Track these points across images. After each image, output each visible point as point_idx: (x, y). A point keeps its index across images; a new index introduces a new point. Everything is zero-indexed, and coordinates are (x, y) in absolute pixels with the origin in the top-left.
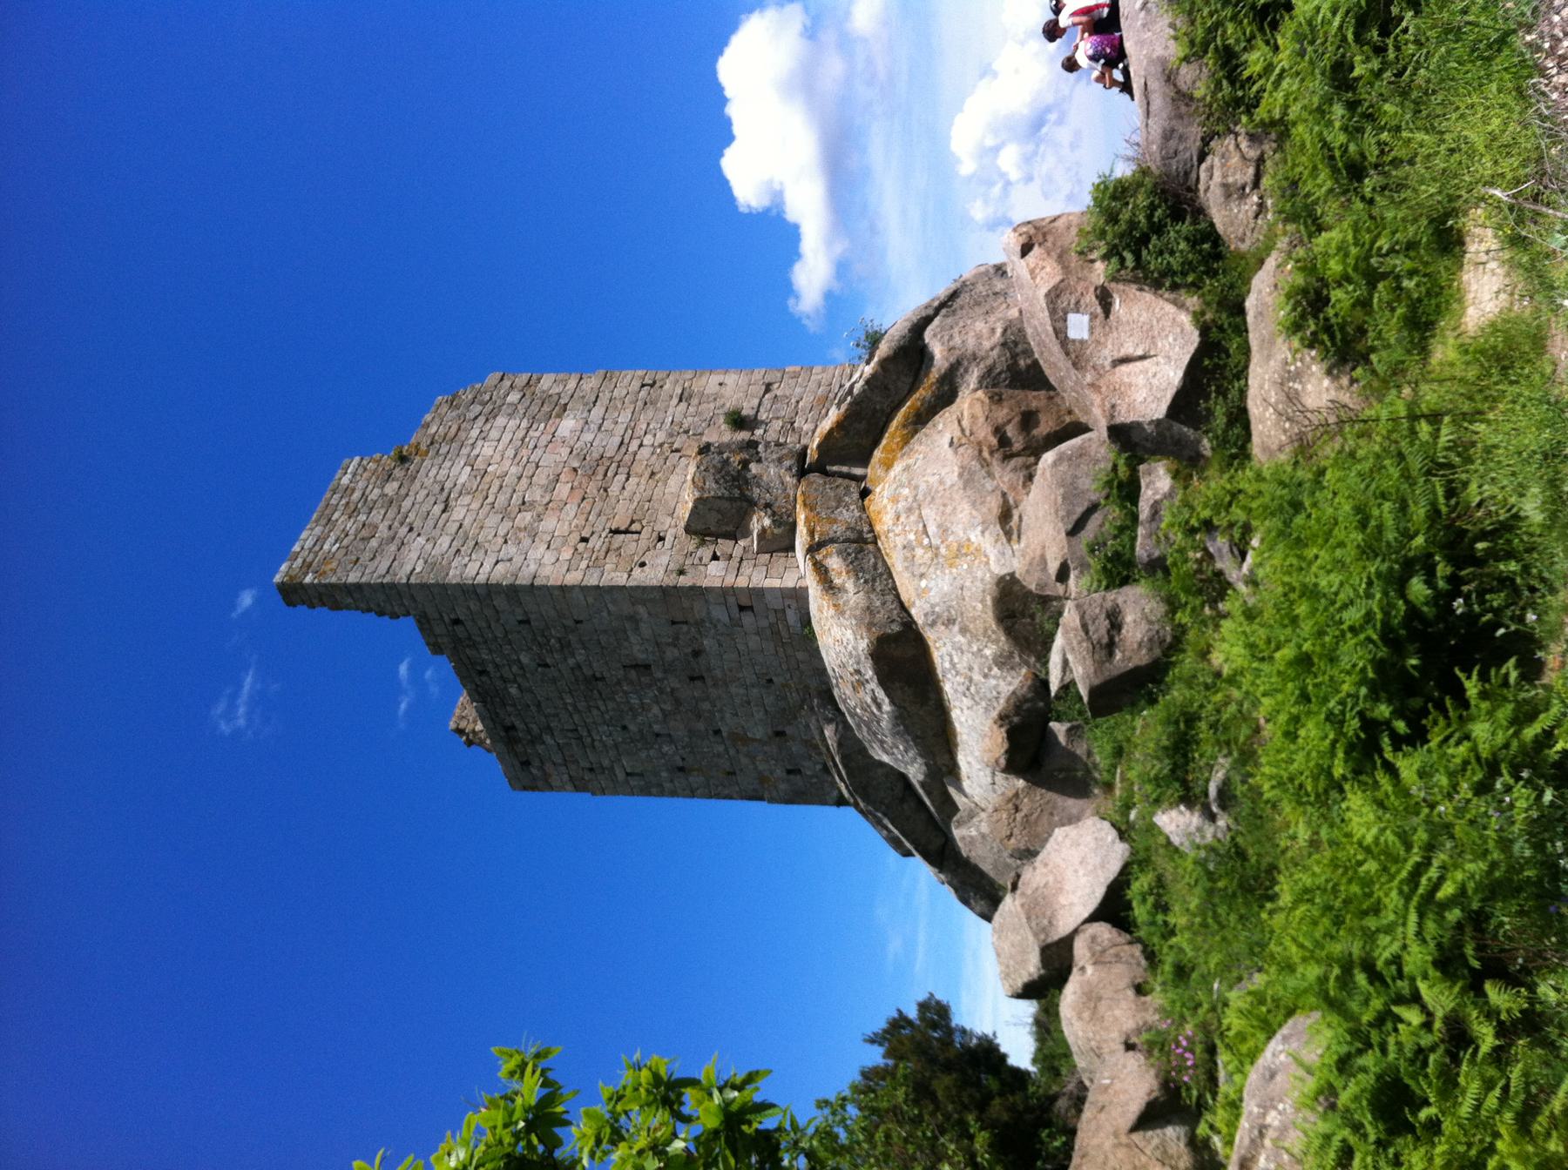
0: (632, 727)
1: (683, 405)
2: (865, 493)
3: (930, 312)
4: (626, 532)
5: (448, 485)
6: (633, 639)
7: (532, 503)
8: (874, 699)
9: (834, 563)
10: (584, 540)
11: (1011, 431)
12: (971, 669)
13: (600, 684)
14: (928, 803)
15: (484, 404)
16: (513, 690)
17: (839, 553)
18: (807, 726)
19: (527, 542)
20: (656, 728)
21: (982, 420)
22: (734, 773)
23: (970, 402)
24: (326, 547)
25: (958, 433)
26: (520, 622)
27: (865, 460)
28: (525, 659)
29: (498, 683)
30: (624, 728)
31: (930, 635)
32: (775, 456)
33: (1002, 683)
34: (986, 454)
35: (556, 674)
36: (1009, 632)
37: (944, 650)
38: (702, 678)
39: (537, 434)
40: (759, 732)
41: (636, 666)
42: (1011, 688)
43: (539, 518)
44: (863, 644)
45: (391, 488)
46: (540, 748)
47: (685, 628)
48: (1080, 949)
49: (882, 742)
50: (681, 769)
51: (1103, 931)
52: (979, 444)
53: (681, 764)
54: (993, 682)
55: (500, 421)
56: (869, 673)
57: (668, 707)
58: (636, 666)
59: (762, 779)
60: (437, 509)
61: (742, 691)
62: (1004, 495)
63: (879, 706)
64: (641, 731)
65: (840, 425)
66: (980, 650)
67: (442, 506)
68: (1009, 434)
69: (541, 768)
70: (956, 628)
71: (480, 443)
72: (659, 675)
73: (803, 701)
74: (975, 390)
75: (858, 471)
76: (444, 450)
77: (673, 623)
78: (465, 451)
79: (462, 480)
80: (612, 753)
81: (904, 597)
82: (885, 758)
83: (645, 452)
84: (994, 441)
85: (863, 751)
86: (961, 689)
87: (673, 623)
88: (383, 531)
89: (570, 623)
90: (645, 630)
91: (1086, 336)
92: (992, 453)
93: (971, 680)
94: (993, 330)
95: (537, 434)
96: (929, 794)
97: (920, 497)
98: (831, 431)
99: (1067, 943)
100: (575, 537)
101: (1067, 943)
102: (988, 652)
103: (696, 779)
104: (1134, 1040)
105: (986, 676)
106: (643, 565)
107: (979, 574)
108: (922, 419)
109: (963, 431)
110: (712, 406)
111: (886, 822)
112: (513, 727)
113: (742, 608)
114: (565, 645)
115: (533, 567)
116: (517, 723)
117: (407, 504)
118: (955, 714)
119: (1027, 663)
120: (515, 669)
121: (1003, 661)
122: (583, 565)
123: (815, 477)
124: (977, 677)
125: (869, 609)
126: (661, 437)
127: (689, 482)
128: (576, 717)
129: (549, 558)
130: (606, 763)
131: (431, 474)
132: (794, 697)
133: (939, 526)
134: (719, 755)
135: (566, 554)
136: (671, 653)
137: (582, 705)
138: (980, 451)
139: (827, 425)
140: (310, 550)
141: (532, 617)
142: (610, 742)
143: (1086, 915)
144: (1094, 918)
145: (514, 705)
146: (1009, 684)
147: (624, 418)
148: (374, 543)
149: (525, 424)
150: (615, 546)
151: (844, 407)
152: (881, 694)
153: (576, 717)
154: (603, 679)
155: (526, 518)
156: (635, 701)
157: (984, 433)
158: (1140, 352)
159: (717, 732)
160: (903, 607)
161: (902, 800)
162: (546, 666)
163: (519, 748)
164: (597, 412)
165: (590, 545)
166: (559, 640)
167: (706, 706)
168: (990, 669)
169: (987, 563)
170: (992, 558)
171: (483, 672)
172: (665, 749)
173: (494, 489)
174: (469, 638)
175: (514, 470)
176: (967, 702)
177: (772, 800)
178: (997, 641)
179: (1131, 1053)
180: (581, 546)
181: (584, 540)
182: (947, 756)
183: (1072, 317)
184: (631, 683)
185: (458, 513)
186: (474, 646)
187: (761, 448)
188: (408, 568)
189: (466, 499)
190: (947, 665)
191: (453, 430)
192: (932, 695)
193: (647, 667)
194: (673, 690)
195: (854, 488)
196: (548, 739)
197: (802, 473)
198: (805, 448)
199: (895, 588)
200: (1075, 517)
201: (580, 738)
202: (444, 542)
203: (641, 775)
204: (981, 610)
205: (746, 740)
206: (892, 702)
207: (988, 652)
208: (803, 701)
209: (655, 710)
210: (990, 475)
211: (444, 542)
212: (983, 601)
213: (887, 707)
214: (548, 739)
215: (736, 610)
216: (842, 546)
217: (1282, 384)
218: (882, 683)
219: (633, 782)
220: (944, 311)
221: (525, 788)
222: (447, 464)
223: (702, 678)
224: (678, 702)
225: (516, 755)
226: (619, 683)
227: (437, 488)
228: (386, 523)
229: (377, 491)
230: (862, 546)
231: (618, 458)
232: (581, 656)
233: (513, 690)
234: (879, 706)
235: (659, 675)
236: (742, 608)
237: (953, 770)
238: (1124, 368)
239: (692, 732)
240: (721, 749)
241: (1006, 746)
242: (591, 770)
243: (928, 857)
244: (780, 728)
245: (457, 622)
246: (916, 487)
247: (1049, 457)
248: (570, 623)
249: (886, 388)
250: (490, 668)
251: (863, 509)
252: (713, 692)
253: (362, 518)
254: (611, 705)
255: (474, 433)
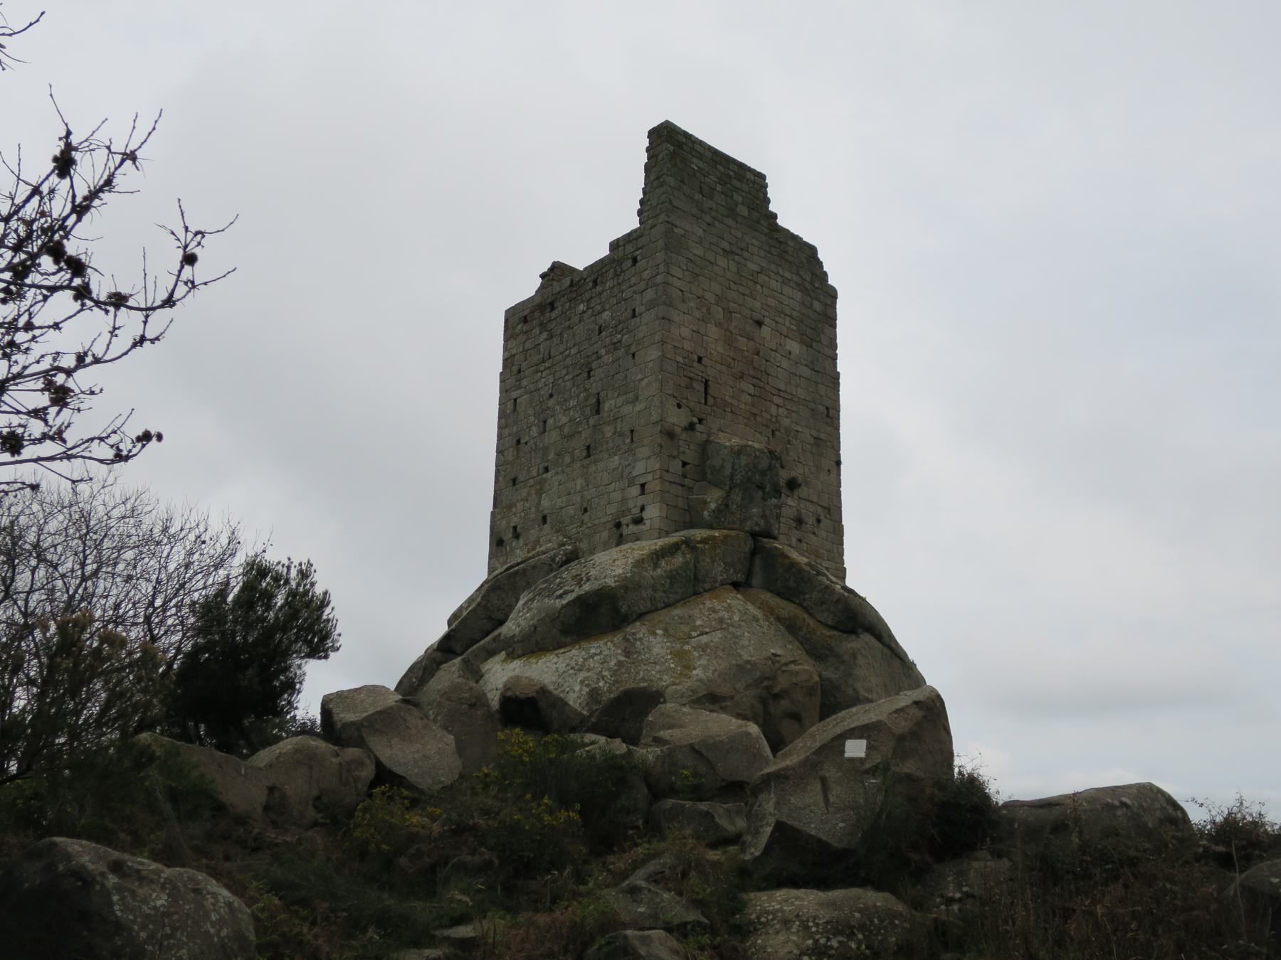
0: (552, 402)
1: (812, 441)
2: (736, 585)
3: (886, 640)
4: (706, 393)
5: (745, 254)
6: (620, 400)
7: (730, 319)
8: (566, 593)
9: (678, 560)
10: (700, 359)
11: (785, 703)
12: (589, 670)
13: (585, 375)
14: (487, 639)
15: (812, 283)
16: (582, 307)
17: (686, 563)
18: (550, 541)
19: (698, 314)
20: (551, 421)
21: (794, 680)
22: (514, 484)
23: (807, 668)
24: (695, 160)
25: (783, 660)
26: (634, 310)
27: (769, 587)
28: (606, 315)
29: (587, 295)
30: (551, 396)
31: (618, 638)
32: (768, 513)
33: (575, 695)
34: (765, 683)
35: (593, 341)
36: (618, 700)
37: (604, 648)
38: (588, 455)
39: (787, 324)
40: (545, 503)
41: (598, 402)
42: (571, 703)
43: (718, 325)
44: (610, 582)
45: (743, 210)
46: (537, 330)
47: (628, 441)
48: (352, 753)
49: (532, 600)
50: (518, 442)
51: (368, 772)
52: (774, 678)
53: (523, 441)
54: (577, 688)
55: (798, 296)
56: (587, 587)
57: (566, 430)
58: (598, 402)
59: (510, 507)
60: (726, 245)
61: (578, 488)
62: (732, 698)
63: (560, 597)
64: (548, 409)
65: (793, 564)
66: (603, 677)
67: (728, 248)
68: (782, 702)
69: (522, 332)
70: (622, 658)
71: (780, 279)
72: (592, 422)
73: (570, 538)
74: (820, 676)
75: (756, 580)
76: (775, 251)
77: (632, 431)
78: (773, 267)
79: (749, 264)
80: (532, 387)
81: (649, 617)
82: (521, 603)
83: (773, 410)
84: (776, 690)
85: (528, 586)
86: (573, 663)
87: (632, 431)
88: (708, 204)
89: (633, 349)
90: (627, 409)
91: (847, 755)
92: (767, 688)
93: (580, 670)
94: (870, 691)
95: (787, 324)
96: (494, 639)
97: (731, 629)
98: (787, 557)
99: (361, 743)
100: (701, 352)
101: (361, 743)
102: (601, 684)
103: (510, 455)
104: (277, 795)
105: (582, 682)
106: (679, 406)
107: (665, 677)
108: (791, 627)
109: (786, 664)
110: (811, 464)
111: (473, 605)
112: (553, 309)
113: (643, 486)
114: (616, 346)
115: (676, 318)
116: (556, 312)
117: (730, 222)
118: (552, 657)
119: (591, 715)
120: (598, 307)
121: (594, 694)
122: (680, 359)
123: (748, 545)
124: (581, 676)
125: (638, 587)
126: (786, 422)
127: (745, 442)
128: (560, 357)
129: (685, 332)
130: (524, 383)
131: (754, 241)
132: (573, 531)
133: (707, 644)
134: (529, 472)
135: (687, 345)
136: (608, 431)
137: (569, 361)
138: (768, 679)
139: (794, 555)
140: (693, 148)
141: (637, 319)
142: (540, 385)
143: (383, 759)
144: (379, 765)
145: (570, 308)
146: (575, 696)
147: (801, 393)
148: (697, 196)
149: (795, 314)
150: (695, 385)
151: (808, 568)
152: (570, 597)
153: (560, 357)
154: (589, 377)
155: (718, 313)
156: (572, 403)
157: (783, 682)
158: (832, 800)
159: (546, 470)
160: (640, 616)
161: (490, 618)
162: (600, 332)
163: (537, 314)
164: (805, 372)
165: (695, 364)
166: (620, 341)
167: (567, 459)
168: (587, 686)
169: (674, 684)
170: (679, 687)
171: (595, 282)
172: (534, 429)
173: (741, 289)
174: (622, 271)
175: (758, 305)
176: (562, 667)
177: (493, 514)
178: (610, 691)
179: (266, 792)
180: (696, 358)
181: (700, 359)
182: (520, 652)
183: (863, 743)
184: (586, 399)
185: (722, 262)
186: (616, 275)
187: (774, 501)
188: (678, 223)
189: (733, 267)
190: (593, 651)
191: (790, 258)
192: (568, 640)
193: (598, 412)
194: (580, 433)
195: (740, 577)
196: (545, 335)
197: (754, 535)
198: (776, 538)
199: (657, 610)
200: (703, 751)
201: (544, 361)
202: (699, 251)
203: (515, 410)
204: (633, 680)
205: (540, 493)
206: (564, 607)
207: (601, 684)
208: (570, 538)
209: (564, 420)
210: (748, 687)
211: (699, 251)
212: (643, 679)
213: (559, 603)
214: (545, 335)
215: (642, 481)
216: (691, 566)
217: (798, 916)
218: (579, 598)
219: (510, 405)
220: (886, 651)
221: (506, 321)
222: (762, 253)
223: (588, 455)
224: (570, 437)
225: (532, 312)
226: (586, 390)
227: (743, 245)
228: (714, 206)
229: (740, 199)
230: (691, 586)
231: (767, 387)
232: (608, 359)
233: (582, 307)
234: (560, 597)
235: (592, 422)
236: (643, 486)
237: (511, 656)
238: (818, 786)
239: (546, 449)
240: (534, 473)
241: (522, 696)
242: (519, 371)
243: (447, 638)
244: (549, 520)
245: (635, 261)
246: (740, 626)
247: (754, 729)
248: (633, 349)
249: (823, 603)
250: (599, 288)
251: (723, 584)
252: (577, 466)
253: (719, 188)
254: (569, 384)
255: (788, 275)
